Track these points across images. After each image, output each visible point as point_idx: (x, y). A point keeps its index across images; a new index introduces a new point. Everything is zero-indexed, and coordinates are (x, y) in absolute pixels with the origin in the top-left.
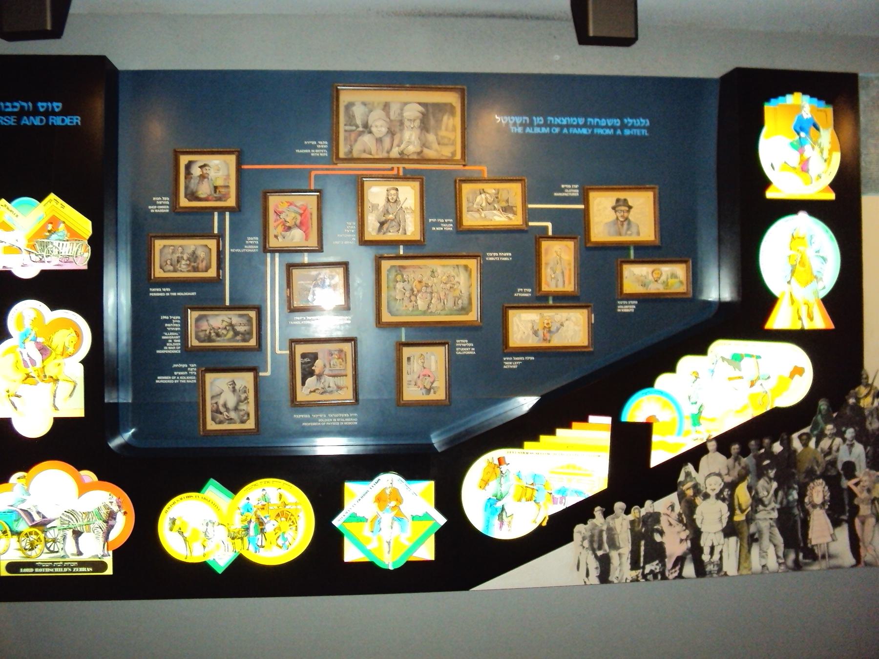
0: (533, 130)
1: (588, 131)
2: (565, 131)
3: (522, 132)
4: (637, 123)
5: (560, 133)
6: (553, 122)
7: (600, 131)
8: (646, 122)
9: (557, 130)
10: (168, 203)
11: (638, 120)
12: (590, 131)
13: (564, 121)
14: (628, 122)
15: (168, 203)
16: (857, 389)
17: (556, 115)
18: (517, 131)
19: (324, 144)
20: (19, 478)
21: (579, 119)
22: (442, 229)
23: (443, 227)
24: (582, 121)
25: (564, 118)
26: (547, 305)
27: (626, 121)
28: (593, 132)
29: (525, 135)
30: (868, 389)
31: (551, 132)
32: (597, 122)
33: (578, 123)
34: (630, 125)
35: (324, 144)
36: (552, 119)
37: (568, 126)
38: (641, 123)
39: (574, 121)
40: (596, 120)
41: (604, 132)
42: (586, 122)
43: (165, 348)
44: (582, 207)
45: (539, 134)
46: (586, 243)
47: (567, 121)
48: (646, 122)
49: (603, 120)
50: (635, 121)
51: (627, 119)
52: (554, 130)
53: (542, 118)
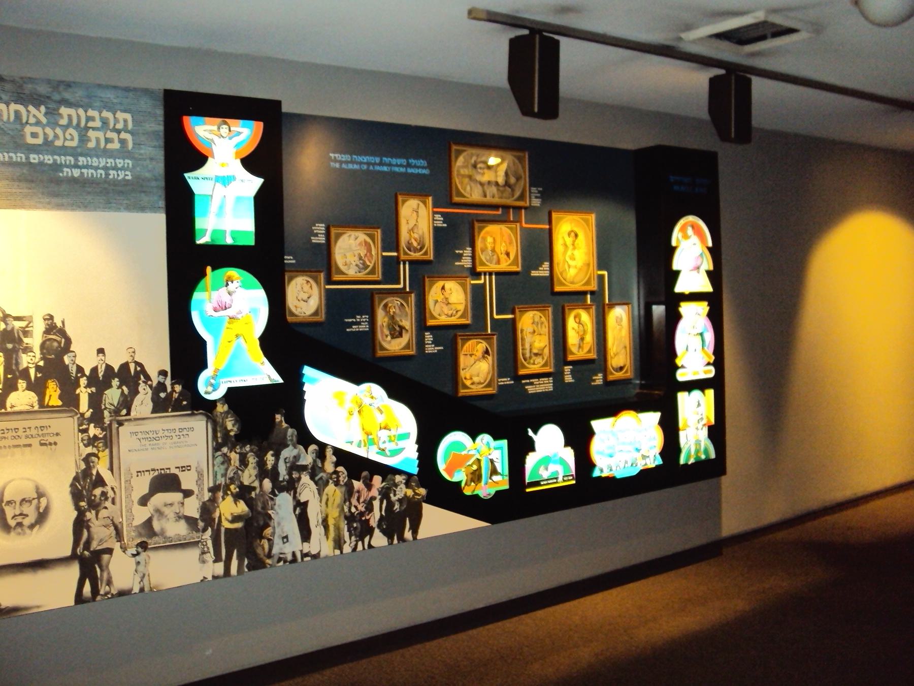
0: (347, 166)
1: (388, 169)
2: (371, 168)
4: (118, 175)
5: (368, 169)
7: (397, 169)
8: (424, 164)
11: (419, 161)
13: (365, 159)
14: (412, 163)
15: (324, 232)
17: (360, 154)
19: (365, 318)
20: (205, 131)
27: (410, 161)
28: (391, 170)
29: (341, 170)
31: (360, 168)
33: (397, 163)
34: (413, 164)
35: (365, 318)
37: (368, 164)
38: (421, 163)
39: (372, 160)
40: (390, 159)
43: (462, 261)
45: (352, 169)
46: (478, 221)
47: (367, 159)
49: (394, 160)
50: (416, 161)
52: (363, 167)
53: (349, 156)
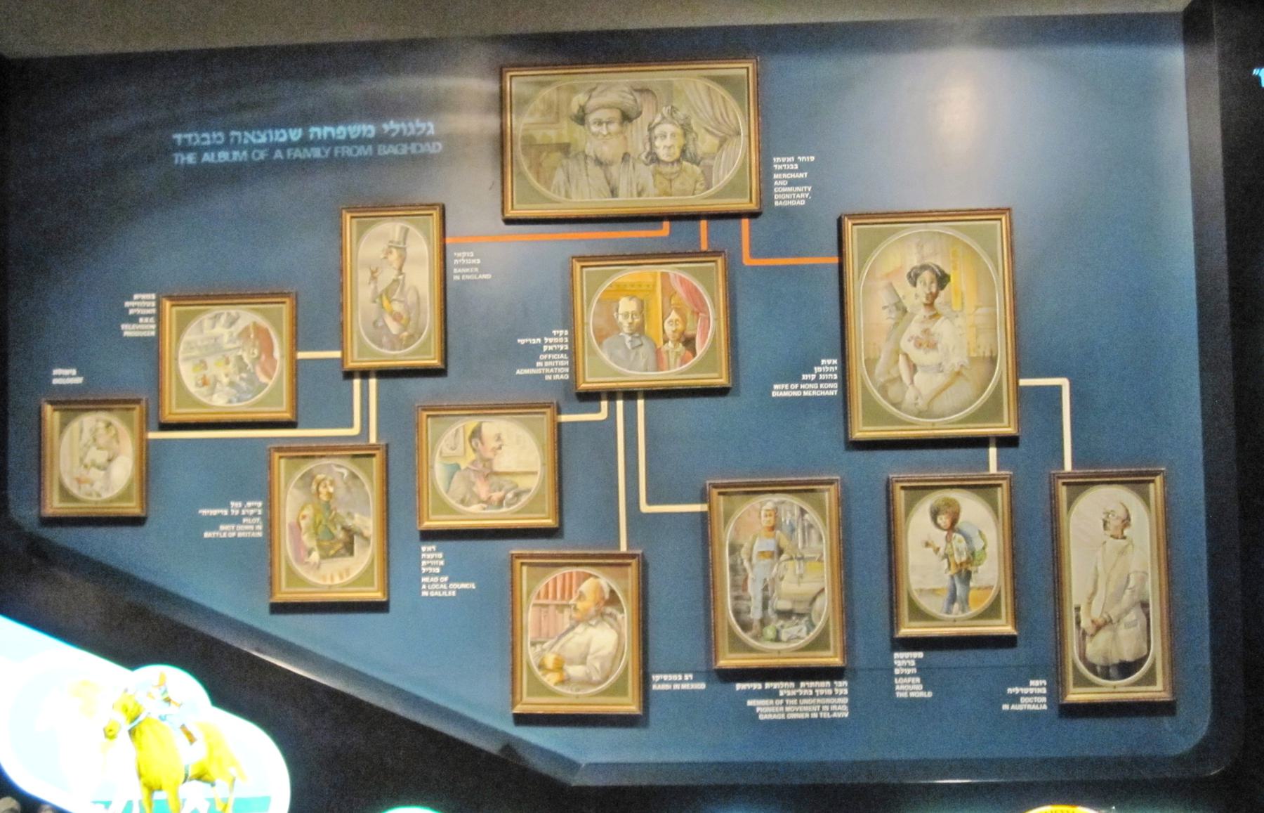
1: (323, 153)
3: (195, 162)
6: (240, 141)
9: (262, 155)
10: (776, 176)
11: (411, 125)
12: (327, 152)
16: (499, 754)
18: (186, 161)
21: (290, 130)
22: (801, 159)
23: (796, 161)
24: (297, 135)
25: (250, 132)
26: (616, 552)
30: (637, 559)
32: (329, 134)
33: (289, 140)
36: (238, 134)
41: (355, 151)
42: (200, 156)
44: (301, 355)
48: (428, 128)
51: (414, 123)
